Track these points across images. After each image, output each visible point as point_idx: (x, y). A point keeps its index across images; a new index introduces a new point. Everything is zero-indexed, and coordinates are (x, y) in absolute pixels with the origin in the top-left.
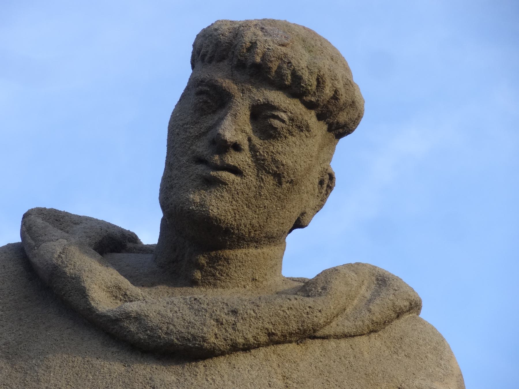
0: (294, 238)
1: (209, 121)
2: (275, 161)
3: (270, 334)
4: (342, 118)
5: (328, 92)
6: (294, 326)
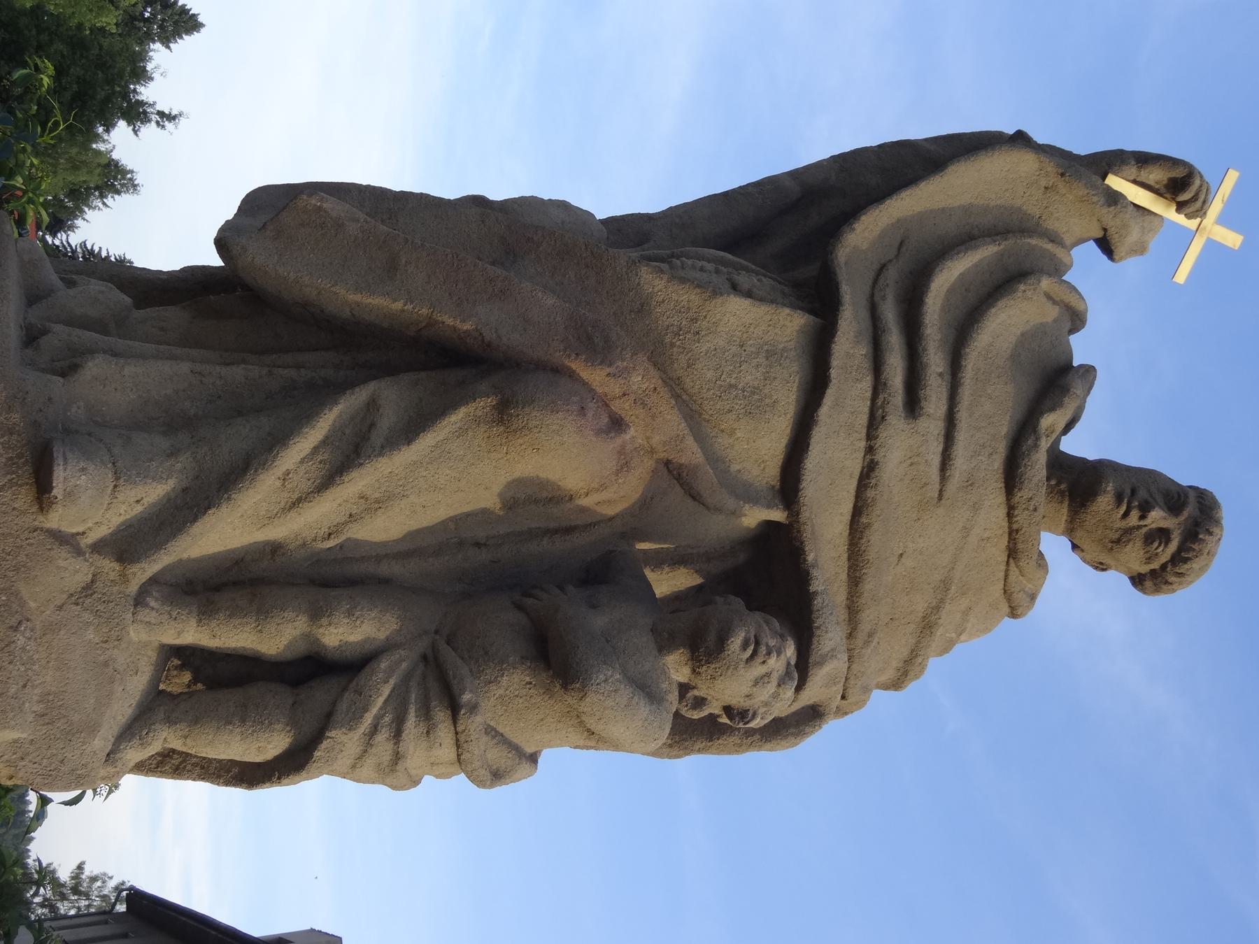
0: (1065, 542)
1: (1160, 500)
2: (1129, 541)
3: (1017, 531)
4: (1148, 584)
5: (1172, 579)
6: (1020, 546)
